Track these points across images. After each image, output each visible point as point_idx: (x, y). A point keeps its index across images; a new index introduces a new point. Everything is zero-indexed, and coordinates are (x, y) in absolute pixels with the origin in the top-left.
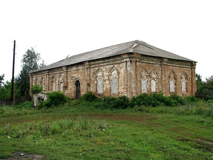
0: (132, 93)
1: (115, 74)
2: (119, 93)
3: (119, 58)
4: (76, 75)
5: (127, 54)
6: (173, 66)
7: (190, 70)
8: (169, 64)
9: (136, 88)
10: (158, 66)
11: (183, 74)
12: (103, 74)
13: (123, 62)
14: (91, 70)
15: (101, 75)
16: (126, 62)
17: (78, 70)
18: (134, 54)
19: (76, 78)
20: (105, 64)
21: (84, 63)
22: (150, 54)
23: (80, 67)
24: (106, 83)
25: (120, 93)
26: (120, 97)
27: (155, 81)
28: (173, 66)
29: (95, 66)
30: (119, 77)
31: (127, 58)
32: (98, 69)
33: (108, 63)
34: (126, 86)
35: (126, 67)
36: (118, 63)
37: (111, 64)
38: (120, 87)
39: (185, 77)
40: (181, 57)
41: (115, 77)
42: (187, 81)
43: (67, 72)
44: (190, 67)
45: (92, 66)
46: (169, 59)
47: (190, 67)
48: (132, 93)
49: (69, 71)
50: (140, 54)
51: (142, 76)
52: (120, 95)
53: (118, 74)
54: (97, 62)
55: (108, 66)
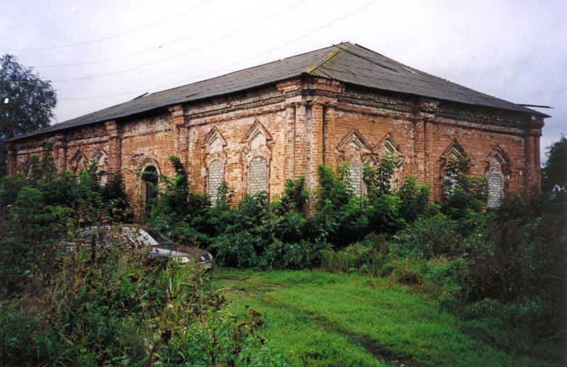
3: (272, 95)
4: (147, 149)
5: (294, 82)
6: (459, 126)
7: (519, 143)
8: (444, 120)
10: (403, 124)
11: (495, 153)
12: (224, 146)
13: (284, 109)
14: (191, 133)
15: (220, 149)
16: (293, 106)
17: (152, 133)
18: (320, 81)
19: (148, 160)
20: (232, 114)
21: (170, 110)
22: (363, 81)
23: (160, 125)
24: (233, 174)
28: (459, 126)
29: (203, 120)
31: (296, 95)
32: (212, 132)
33: (240, 112)
35: (292, 124)
36: (270, 112)
37: (249, 116)
38: (272, 187)
39: (502, 166)
40: (493, 99)
41: (261, 157)
42: (508, 177)
43: (119, 139)
44: (520, 131)
45: (193, 122)
46: (444, 103)
47: (520, 131)
49: (127, 137)
50: (342, 82)
51: (347, 154)
53: (270, 148)
54: (208, 109)
55: (241, 122)
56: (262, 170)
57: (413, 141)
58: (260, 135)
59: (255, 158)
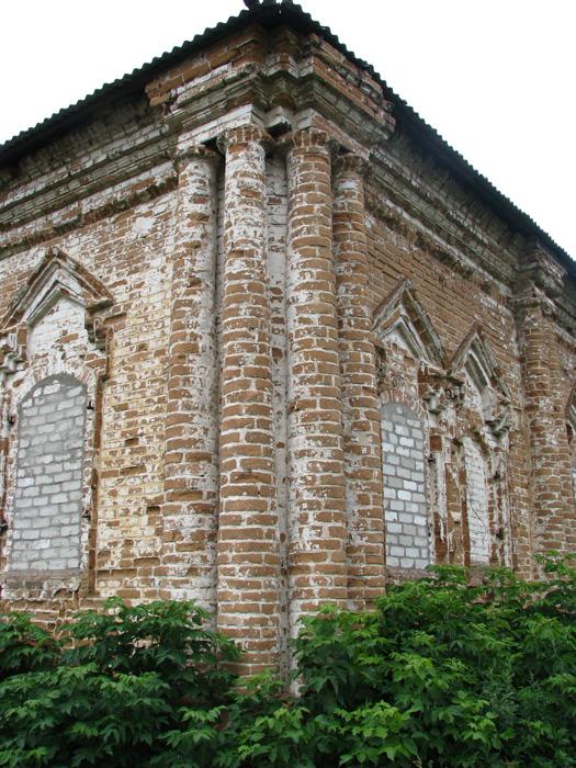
0: (289, 565)
1: (66, 338)
2: (95, 569)
5: (225, 52)
9: (333, 493)
25: (114, 562)
26: (108, 623)
30: (108, 363)
31: (230, 107)
34: (196, 458)
35: (203, 218)
36: (110, 210)
37: (28, 243)
38: (107, 484)
48: (289, 565)
52: (108, 589)
56: (64, 426)
58: (63, 305)
59: (42, 384)
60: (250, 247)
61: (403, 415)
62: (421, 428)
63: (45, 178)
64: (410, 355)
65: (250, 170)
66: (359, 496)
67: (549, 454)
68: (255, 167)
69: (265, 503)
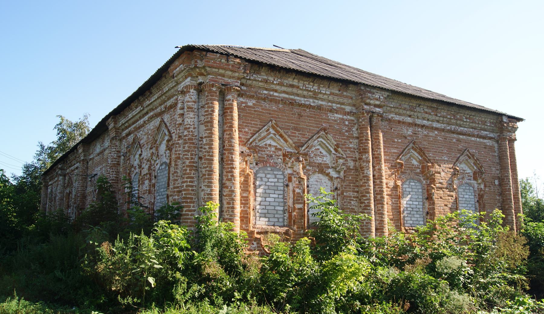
7: (491, 148)
27: (331, 179)
39: (475, 173)
42: (482, 186)
44: (492, 135)
57: (357, 141)
60: (189, 126)
61: (271, 170)
62: (283, 174)
63: (157, 95)
64: (279, 147)
65: (190, 100)
66: (227, 202)
67: (365, 178)
68: (191, 99)
69: (190, 206)
